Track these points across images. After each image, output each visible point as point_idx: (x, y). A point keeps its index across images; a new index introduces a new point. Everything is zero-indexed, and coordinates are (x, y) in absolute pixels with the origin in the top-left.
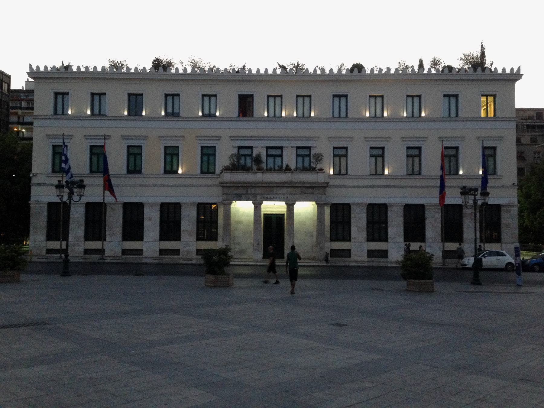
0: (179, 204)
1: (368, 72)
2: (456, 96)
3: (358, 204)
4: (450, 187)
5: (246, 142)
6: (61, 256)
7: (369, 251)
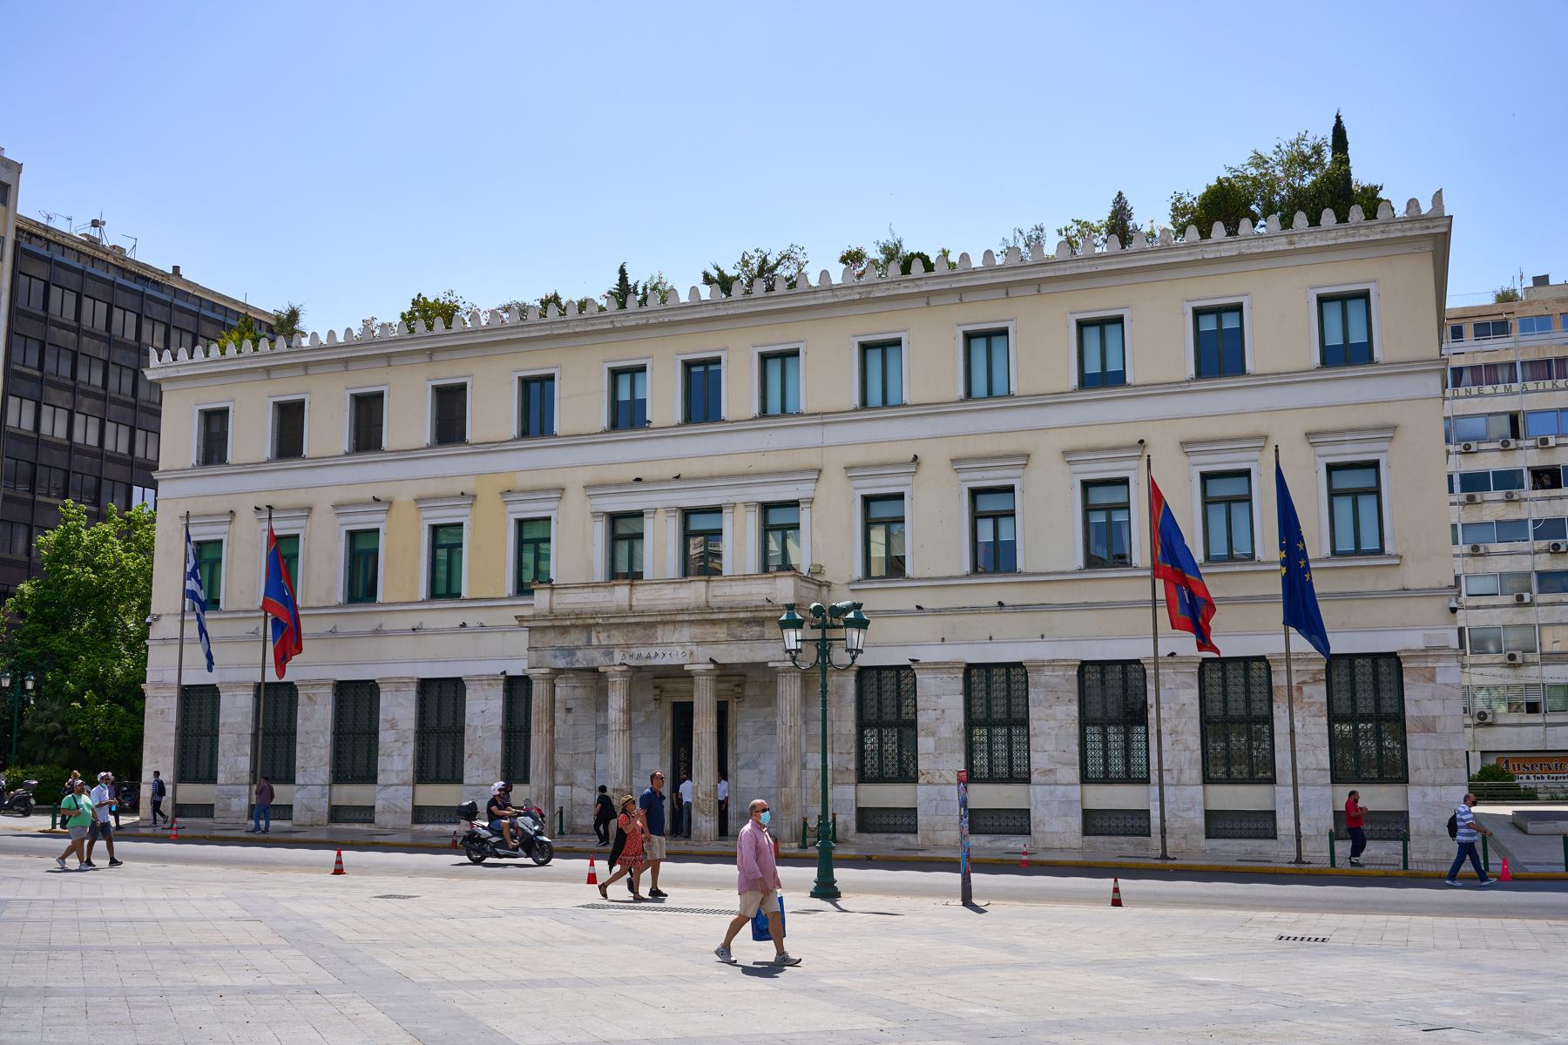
1: (1400, 211)
3: (937, 667)
6: (257, 824)
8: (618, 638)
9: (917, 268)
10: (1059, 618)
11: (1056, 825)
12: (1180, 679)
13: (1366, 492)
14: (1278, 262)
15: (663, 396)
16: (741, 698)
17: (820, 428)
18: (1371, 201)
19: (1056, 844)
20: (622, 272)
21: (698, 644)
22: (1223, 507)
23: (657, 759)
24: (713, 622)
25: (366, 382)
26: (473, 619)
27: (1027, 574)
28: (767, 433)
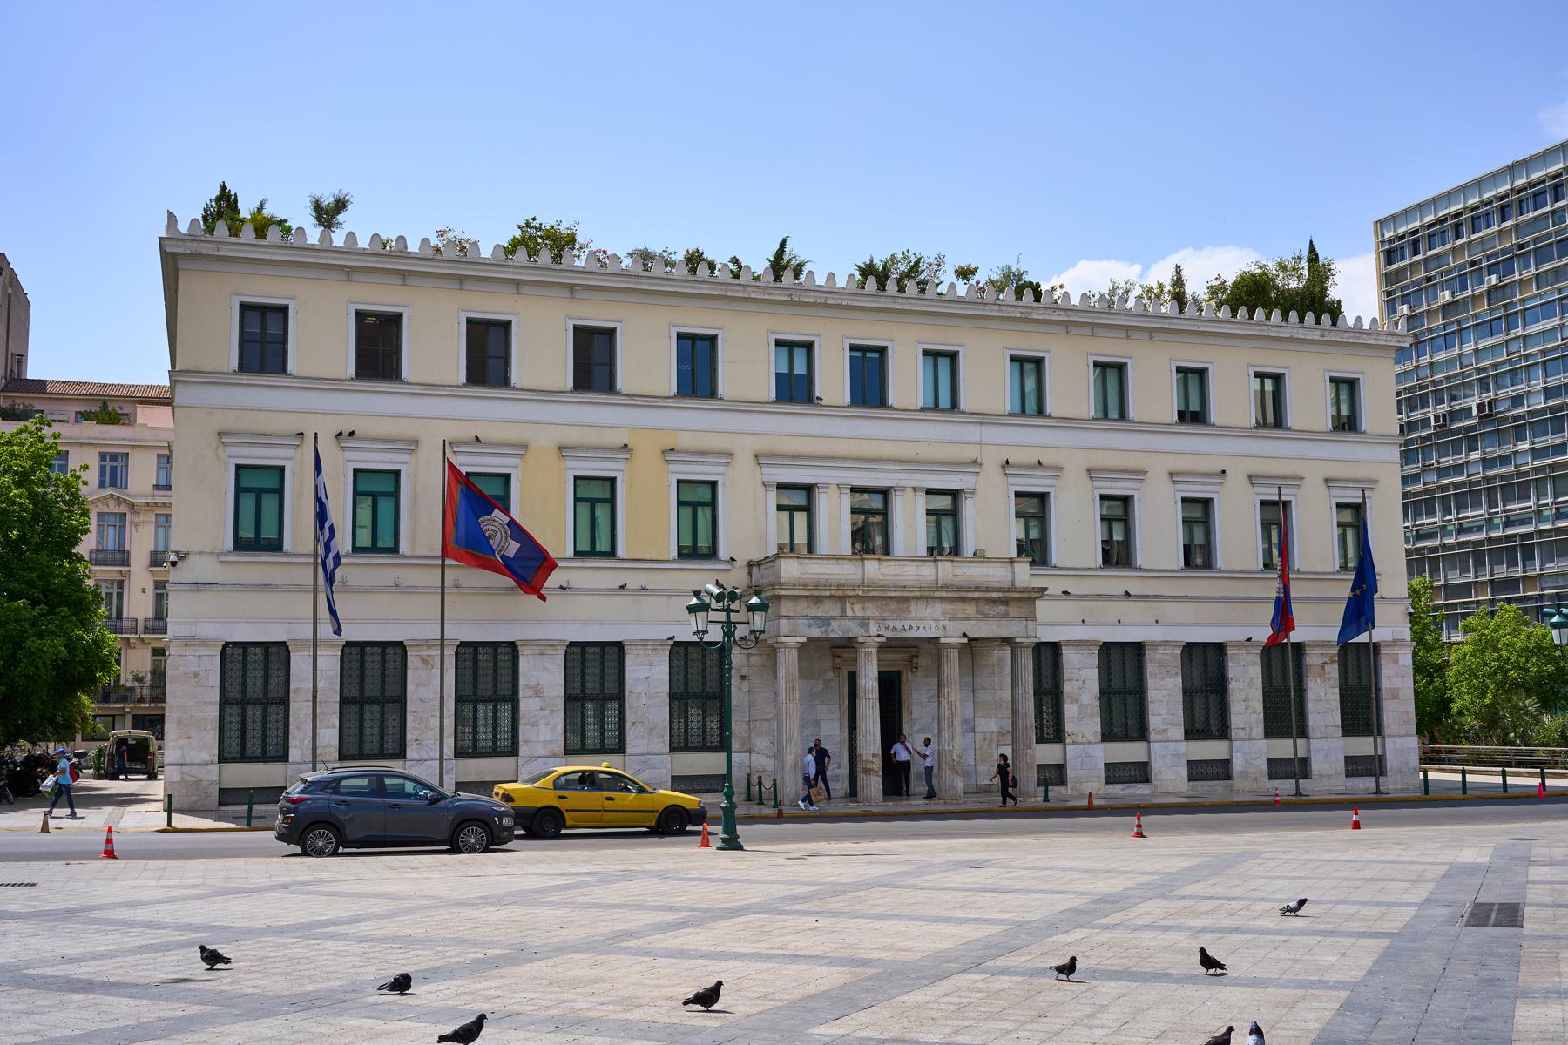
0: (400, 645)
2: (953, 356)
3: (1079, 644)
4: (1307, 600)
5: (947, 477)
7: (1109, 767)
8: (872, 610)
9: (1028, 296)
10: (1168, 607)
11: (1170, 776)
12: (1250, 658)
13: (704, 504)
14: (1306, 347)
15: (833, 379)
16: (914, 668)
17: (978, 428)
18: (1335, 311)
19: (1170, 789)
20: (783, 244)
21: (951, 618)
22: (370, 500)
23: (837, 725)
24: (963, 600)
25: (381, 299)
26: (634, 580)
27: (406, 557)
28: (932, 425)
